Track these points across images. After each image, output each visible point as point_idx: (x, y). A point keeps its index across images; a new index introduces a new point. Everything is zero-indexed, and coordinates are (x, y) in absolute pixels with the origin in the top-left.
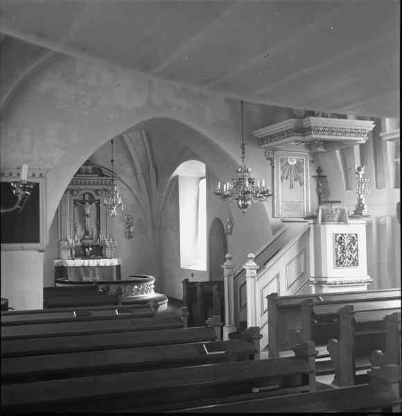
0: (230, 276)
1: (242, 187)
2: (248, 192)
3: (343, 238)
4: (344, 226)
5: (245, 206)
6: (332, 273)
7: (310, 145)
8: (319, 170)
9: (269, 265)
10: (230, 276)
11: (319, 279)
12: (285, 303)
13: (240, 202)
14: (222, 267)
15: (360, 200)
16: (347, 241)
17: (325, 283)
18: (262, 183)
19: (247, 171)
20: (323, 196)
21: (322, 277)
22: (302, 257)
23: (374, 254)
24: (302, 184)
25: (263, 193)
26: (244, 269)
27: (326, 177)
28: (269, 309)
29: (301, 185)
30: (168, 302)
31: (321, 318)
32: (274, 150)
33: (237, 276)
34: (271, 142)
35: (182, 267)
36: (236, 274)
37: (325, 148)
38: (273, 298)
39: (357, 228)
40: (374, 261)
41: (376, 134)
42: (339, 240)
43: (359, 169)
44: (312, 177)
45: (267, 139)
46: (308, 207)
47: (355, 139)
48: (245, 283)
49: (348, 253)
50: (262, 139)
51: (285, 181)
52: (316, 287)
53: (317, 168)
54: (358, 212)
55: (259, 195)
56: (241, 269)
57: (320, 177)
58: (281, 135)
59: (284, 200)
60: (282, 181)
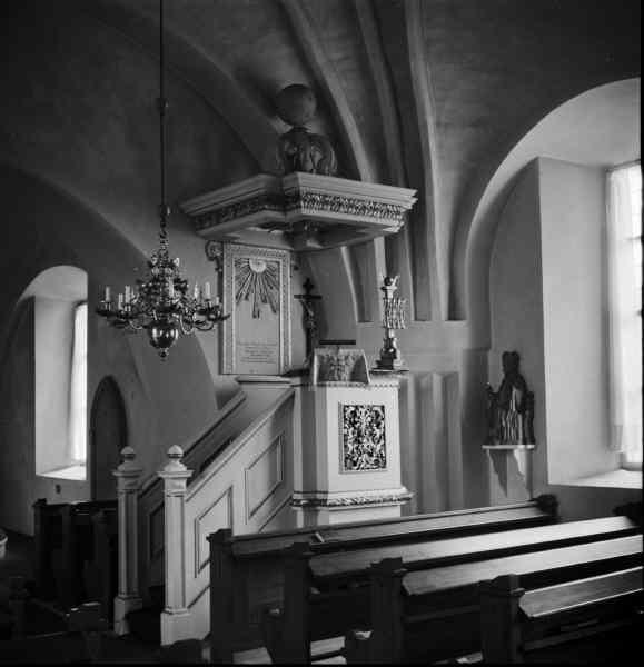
0: (131, 492)
1: (160, 298)
2: (173, 309)
3: (358, 414)
4: (362, 390)
5: (165, 342)
6: (340, 484)
7: (293, 233)
8: (308, 285)
9: (214, 467)
10: (131, 492)
11: (311, 496)
12: (249, 549)
13: (155, 331)
14: (115, 474)
15: (389, 341)
16: (365, 420)
17: (323, 503)
18: (202, 289)
19: (172, 266)
20: (316, 330)
21: (316, 492)
22: (279, 450)
23: (412, 442)
24: (275, 310)
25: (206, 312)
26: (160, 479)
27: (320, 297)
28: (211, 559)
29: (275, 312)
30: (7, 544)
31: (324, 583)
32: (224, 240)
33: (145, 493)
34: (218, 223)
35: (38, 472)
36: (145, 487)
37: (321, 243)
38: (220, 540)
39: (383, 394)
40: (412, 452)
41: (417, 218)
42: (351, 417)
43: (387, 282)
44: (296, 296)
45: (210, 219)
46: (286, 354)
47: (379, 222)
48: (163, 504)
49: (366, 443)
50: (200, 216)
51: (243, 302)
52: (304, 511)
53: (305, 281)
54: (386, 363)
55: (196, 317)
56: (154, 479)
57: (311, 298)
58: (237, 209)
59: (243, 341)
60: (237, 304)
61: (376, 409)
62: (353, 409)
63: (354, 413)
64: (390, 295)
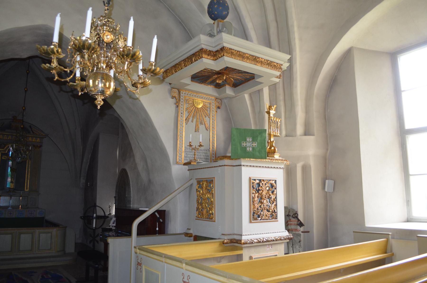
19: (74, 44)
29: (207, 129)
43: (270, 108)
61: (271, 182)
62: (258, 181)
63: (259, 184)
64: (271, 115)
